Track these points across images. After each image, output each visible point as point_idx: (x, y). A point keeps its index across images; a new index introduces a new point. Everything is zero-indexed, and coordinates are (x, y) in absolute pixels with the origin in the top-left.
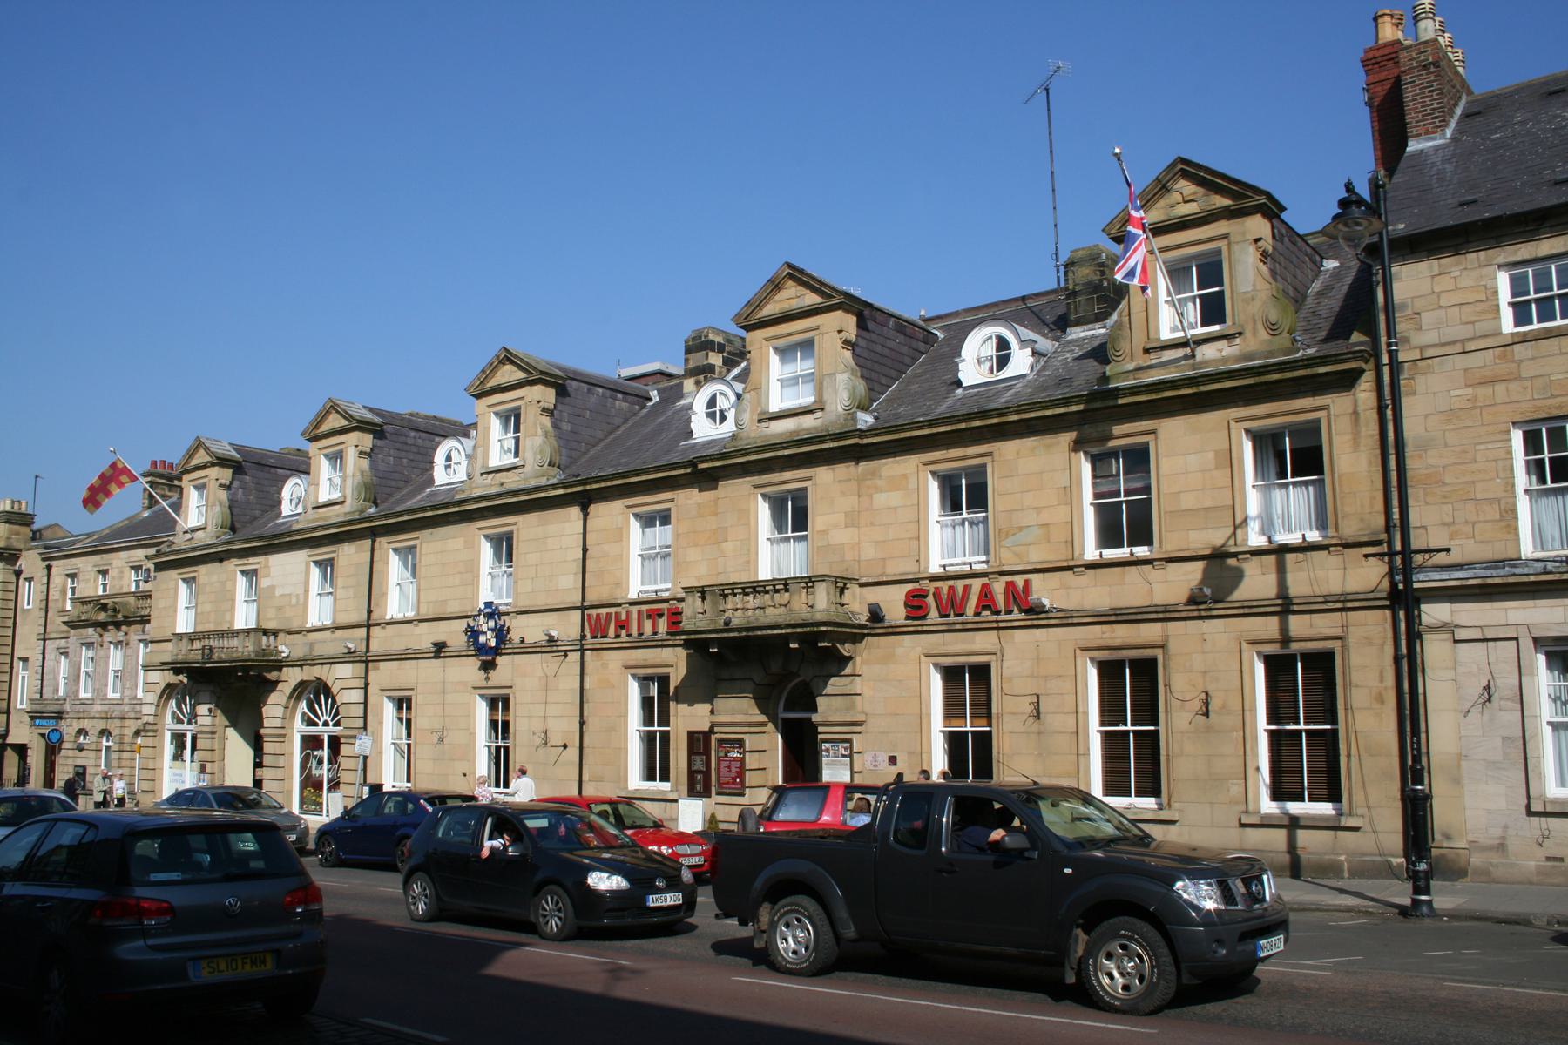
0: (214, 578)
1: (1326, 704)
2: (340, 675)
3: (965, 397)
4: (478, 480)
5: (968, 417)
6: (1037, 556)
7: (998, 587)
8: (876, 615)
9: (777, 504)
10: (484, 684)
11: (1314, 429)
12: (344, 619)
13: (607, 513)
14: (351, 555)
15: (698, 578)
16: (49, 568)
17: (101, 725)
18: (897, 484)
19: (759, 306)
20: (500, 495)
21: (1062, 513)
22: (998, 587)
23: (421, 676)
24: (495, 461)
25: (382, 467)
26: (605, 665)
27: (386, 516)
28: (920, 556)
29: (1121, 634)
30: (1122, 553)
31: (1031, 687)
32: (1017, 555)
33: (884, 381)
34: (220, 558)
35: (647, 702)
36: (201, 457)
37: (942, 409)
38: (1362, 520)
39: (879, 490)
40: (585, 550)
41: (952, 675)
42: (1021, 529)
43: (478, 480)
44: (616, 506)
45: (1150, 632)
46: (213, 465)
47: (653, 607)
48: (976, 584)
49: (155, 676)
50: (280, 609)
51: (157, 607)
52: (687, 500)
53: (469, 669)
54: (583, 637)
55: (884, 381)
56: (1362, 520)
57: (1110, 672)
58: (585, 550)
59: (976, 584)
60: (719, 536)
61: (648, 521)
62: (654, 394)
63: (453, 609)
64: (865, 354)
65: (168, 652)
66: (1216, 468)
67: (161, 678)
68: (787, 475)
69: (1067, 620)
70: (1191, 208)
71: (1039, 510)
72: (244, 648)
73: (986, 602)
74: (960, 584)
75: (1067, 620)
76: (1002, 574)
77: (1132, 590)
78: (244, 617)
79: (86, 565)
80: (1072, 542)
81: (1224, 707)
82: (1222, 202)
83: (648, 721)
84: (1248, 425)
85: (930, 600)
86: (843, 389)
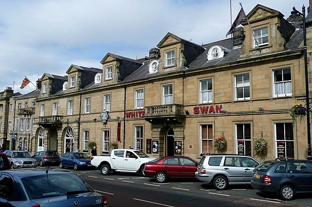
0: (48, 104)
1: (290, 135)
2: (74, 126)
3: (208, 63)
4: (103, 82)
5: (209, 67)
6: (223, 100)
7: (215, 107)
8: (187, 113)
9: (166, 87)
10: (105, 128)
11: (289, 69)
12: (75, 113)
13: (130, 90)
14: (76, 99)
15: (149, 105)
16: (15, 102)
17: (25, 136)
18: (193, 83)
19: (163, 43)
20: (107, 86)
21: (229, 90)
22: (215, 107)
23: (91, 126)
24: (107, 79)
25: (84, 80)
26: (129, 124)
27: (84, 91)
28: (197, 101)
29: (242, 118)
30: (242, 99)
31: (222, 130)
32: (219, 99)
33: (191, 59)
34: (49, 100)
35: (138, 132)
36: (170, 40)
37: (203, 66)
38: (300, 91)
39: (188, 85)
40: (125, 98)
41: (204, 127)
42: (219, 93)
43: (103, 82)
44: (132, 88)
45: (249, 117)
46: (115, 61)
47: (141, 112)
48: (209, 106)
49: (36, 126)
50: (61, 111)
51: (37, 110)
52: (149, 86)
53: (101, 125)
54: (125, 117)
55: (191, 59)
56: (300, 91)
57: (240, 127)
58: (125, 98)
59: (209, 106)
60: (153, 95)
61: (138, 91)
62: (143, 64)
63: (97, 111)
64: (186, 53)
65: (38, 121)
66: (265, 79)
67: (37, 126)
68: (169, 81)
69: (229, 114)
70: (261, 16)
71: (224, 89)
72: (53, 120)
73: (212, 110)
74: (206, 106)
75: (229, 114)
76: (215, 104)
77: (245, 108)
78: (55, 114)
79: (23, 101)
80: (232, 96)
81: (266, 135)
82: (269, 14)
83: (138, 136)
84: (272, 68)
85: (200, 109)
86: (180, 61)
